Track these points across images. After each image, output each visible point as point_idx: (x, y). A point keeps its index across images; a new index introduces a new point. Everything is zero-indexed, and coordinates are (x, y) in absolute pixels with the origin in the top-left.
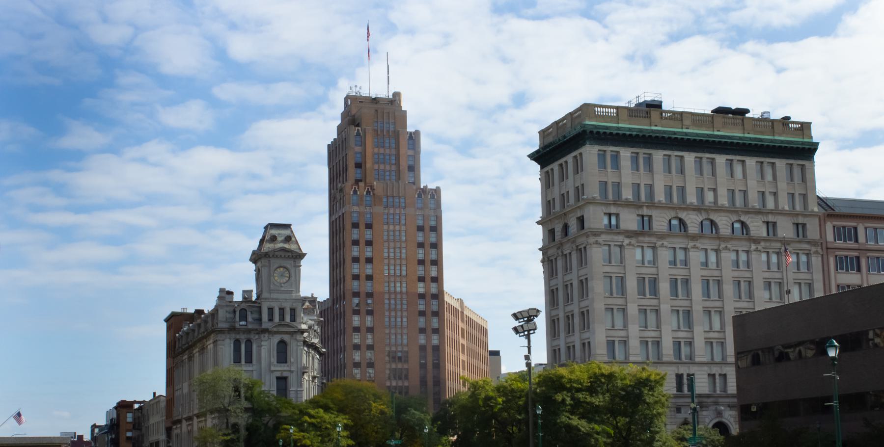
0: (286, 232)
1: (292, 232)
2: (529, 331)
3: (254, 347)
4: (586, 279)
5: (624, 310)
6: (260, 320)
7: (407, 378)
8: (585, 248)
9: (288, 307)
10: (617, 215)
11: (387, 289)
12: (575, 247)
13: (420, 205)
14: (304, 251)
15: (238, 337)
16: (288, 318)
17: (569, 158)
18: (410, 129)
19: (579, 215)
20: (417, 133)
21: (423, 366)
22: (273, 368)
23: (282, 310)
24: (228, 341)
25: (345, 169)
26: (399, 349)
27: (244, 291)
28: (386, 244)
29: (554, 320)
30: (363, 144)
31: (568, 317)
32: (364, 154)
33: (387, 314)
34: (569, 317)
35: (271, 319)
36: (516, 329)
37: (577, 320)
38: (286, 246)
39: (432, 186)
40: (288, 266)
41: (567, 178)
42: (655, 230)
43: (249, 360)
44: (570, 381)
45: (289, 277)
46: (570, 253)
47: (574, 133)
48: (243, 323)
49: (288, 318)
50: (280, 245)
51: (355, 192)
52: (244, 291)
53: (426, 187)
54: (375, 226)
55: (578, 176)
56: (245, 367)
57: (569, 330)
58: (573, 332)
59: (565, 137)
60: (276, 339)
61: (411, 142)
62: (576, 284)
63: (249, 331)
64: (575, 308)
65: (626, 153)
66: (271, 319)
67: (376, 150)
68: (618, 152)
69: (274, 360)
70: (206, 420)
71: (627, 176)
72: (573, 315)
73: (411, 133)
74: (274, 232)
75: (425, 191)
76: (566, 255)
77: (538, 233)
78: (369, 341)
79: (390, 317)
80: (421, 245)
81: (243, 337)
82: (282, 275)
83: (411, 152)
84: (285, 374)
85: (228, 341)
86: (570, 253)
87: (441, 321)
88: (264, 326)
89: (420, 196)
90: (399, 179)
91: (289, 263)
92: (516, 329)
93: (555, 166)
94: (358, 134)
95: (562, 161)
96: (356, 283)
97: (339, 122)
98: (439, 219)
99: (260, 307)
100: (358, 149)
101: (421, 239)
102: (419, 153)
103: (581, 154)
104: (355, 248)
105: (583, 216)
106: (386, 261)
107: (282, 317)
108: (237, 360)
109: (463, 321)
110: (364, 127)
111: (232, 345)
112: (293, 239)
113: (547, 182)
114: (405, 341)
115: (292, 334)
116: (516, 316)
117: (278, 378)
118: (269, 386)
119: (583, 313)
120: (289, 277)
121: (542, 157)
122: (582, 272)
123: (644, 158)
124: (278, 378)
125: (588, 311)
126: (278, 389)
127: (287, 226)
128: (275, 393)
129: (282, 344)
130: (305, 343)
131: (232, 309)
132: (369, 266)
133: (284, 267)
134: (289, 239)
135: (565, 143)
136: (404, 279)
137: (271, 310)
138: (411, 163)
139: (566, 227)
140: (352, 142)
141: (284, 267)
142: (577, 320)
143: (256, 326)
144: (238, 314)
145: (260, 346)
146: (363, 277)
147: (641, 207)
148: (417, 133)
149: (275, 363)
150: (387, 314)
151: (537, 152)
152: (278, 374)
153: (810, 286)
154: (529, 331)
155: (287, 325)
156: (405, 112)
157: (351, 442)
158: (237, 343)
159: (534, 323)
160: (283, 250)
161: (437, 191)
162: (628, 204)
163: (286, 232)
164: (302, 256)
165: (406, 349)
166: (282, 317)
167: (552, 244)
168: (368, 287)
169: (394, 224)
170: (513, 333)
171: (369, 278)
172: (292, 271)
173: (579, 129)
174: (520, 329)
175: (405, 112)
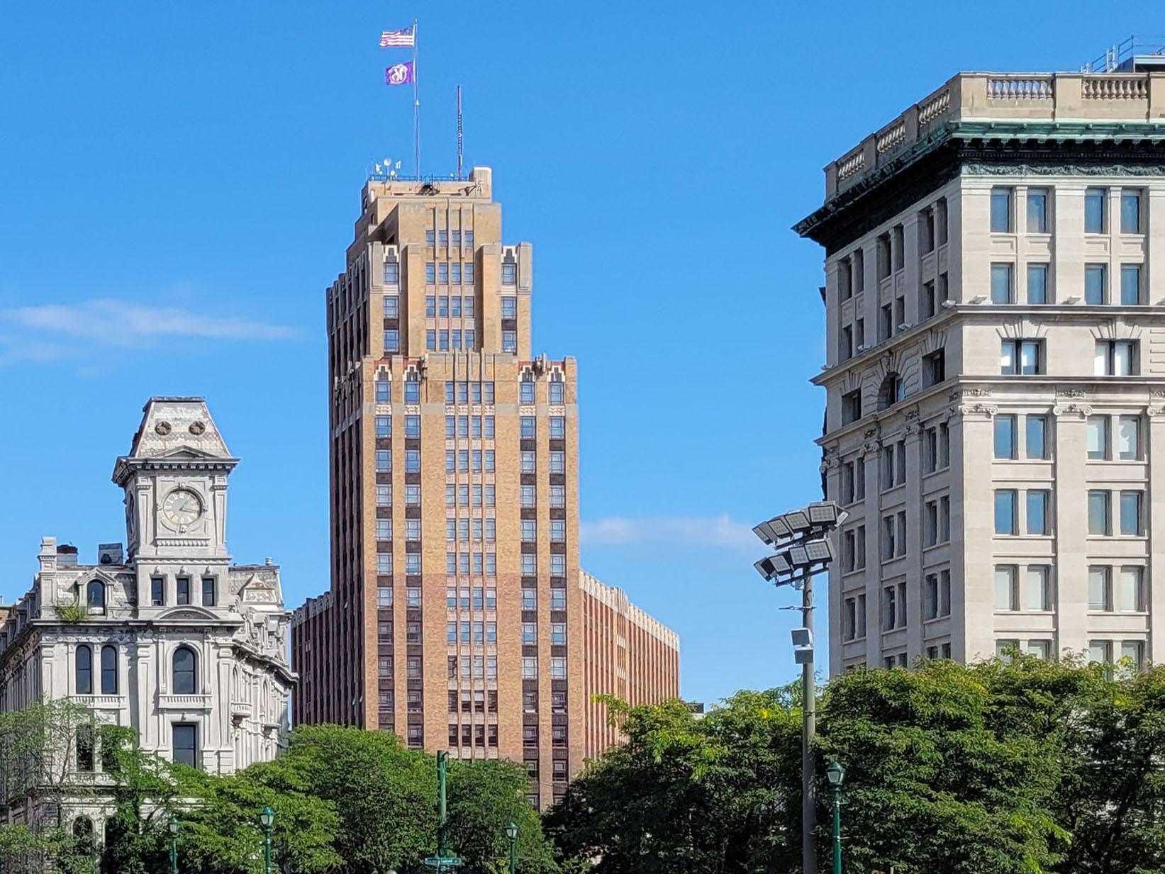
2: (806, 567)
3: (123, 660)
4: (946, 499)
5: (1049, 573)
7: (494, 741)
8: (944, 426)
9: (196, 573)
10: (1039, 344)
12: (915, 427)
15: (83, 639)
16: (197, 599)
17: (909, 218)
19: (931, 348)
21: (531, 723)
22: (162, 704)
23: (184, 582)
25: (364, 334)
26: (479, 686)
27: (101, 547)
29: (850, 602)
31: (889, 591)
34: (893, 594)
36: (767, 566)
37: (915, 595)
38: (193, 444)
40: (198, 487)
41: (901, 265)
42: (1143, 374)
43: (111, 686)
44: (935, 697)
45: (201, 511)
46: (901, 444)
47: (927, 148)
48: (99, 610)
49: (197, 599)
51: (383, 375)
52: (101, 547)
54: (425, 444)
55: (928, 257)
56: (100, 701)
57: (893, 618)
58: (904, 622)
59: (899, 164)
60: (169, 646)
62: (914, 512)
63: (108, 628)
64: (911, 570)
65: (1070, 190)
67: (431, 291)
68: (1049, 190)
69: (167, 686)
70: (25, 812)
71: (1075, 247)
72: (903, 586)
76: (889, 450)
77: (817, 405)
81: (97, 640)
84: (190, 717)
86: (901, 444)
88: (143, 616)
90: (482, 345)
92: (767, 566)
93: (868, 243)
94: (390, 261)
95: (888, 226)
99: (135, 577)
103: (942, 202)
105: (942, 352)
109: (621, 630)
110: (403, 241)
111: (73, 657)
113: (848, 281)
115: (201, 631)
116: (766, 532)
117: (175, 725)
118: (157, 739)
119: (931, 580)
120: (201, 511)
121: (832, 227)
122: (933, 484)
123: (1123, 197)
124: (175, 725)
125: (946, 573)
126: (176, 748)
128: (169, 757)
129: (184, 652)
130: (239, 652)
133: (188, 491)
135: (899, 180)
137: (159, 582)
139: (891, 386)
140: (378, 275)
141: (188, 491)
142: (915, 595)
143: (126, 616)
144: (83, 591)
145: (134, 660)
147: (1109, 320)
149: (170, 693)
151: (819, 214)
152: (177, 717)
154: (806, 567)
155: (196, 614)
157: (337, 860)
158: (84, 651)
160: (189, 453)
162: (1070, 316)
165: (492, 686)
167: (853, 426)
170: (758, 575)
173: (939, 138)
174: (780, 564)
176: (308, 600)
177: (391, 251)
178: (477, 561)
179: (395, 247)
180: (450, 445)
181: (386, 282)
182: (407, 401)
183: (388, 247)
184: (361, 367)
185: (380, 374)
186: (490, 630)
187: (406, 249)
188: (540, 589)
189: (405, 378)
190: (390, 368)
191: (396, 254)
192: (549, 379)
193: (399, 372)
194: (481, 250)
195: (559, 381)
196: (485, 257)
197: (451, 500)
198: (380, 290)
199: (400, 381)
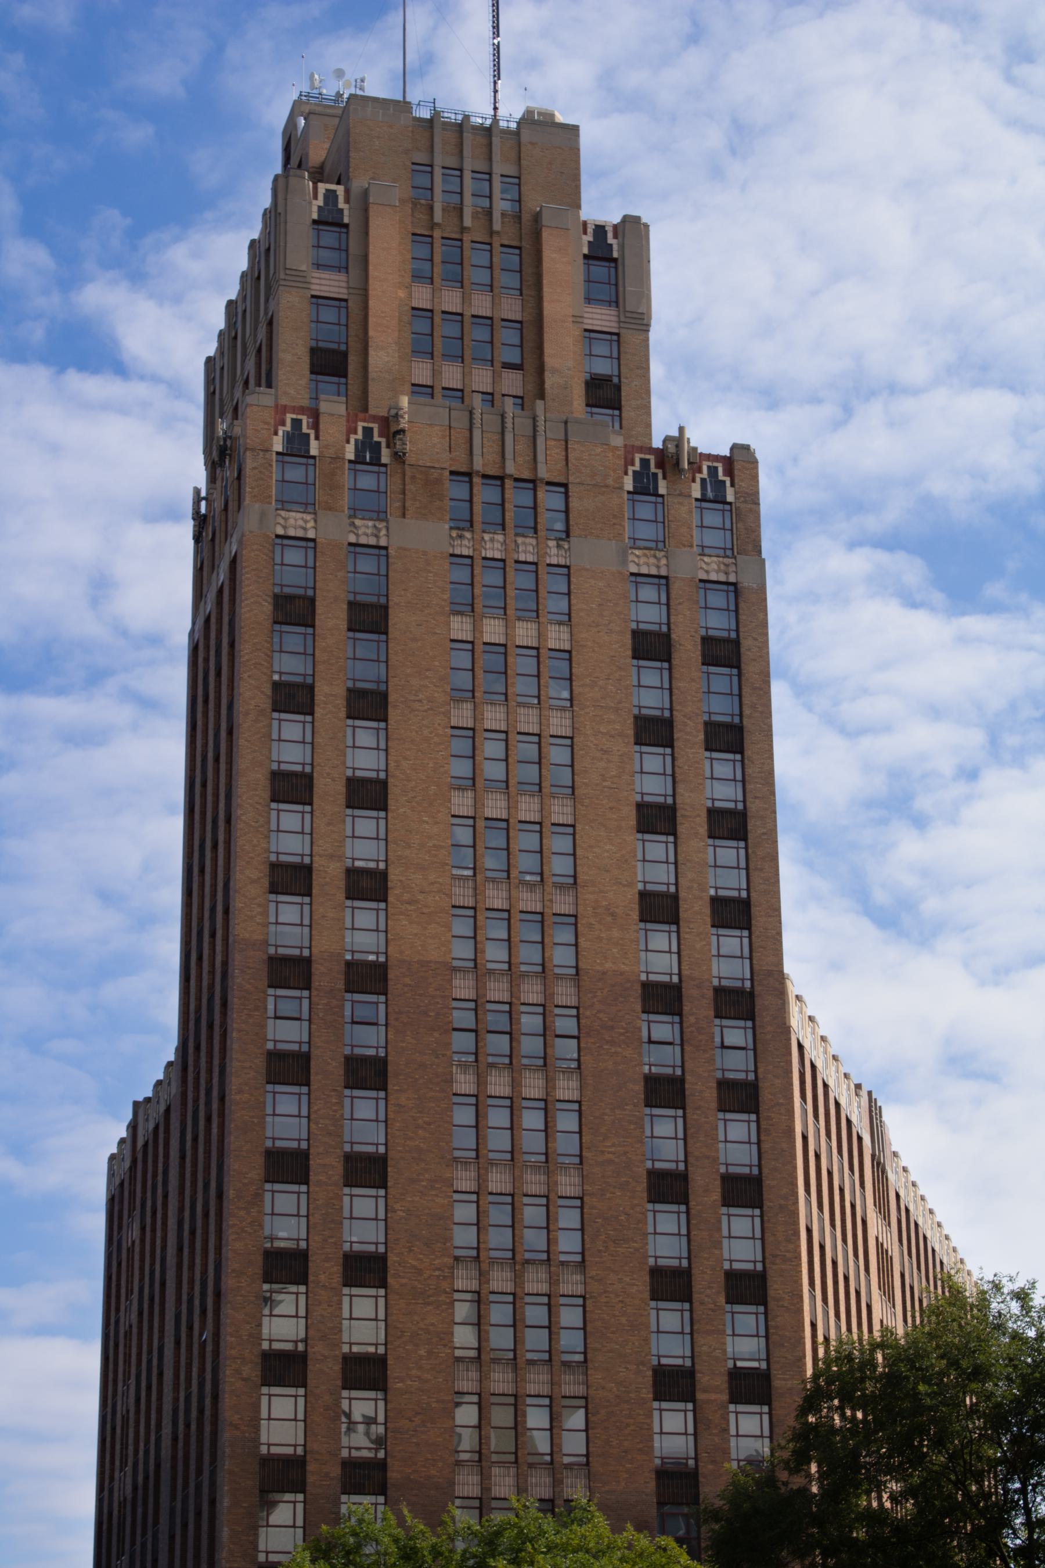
11: (463, 951)
13: (646, 531)
18: (599, 207)
20: (633, 229)
28: (464, 1280)
30: (355, 262)
32: (354, 309)
33: (465, 1083)
39: (710, 435)
53: (678, 441)
54: (398, 619)
61: (600, 270)
67: (422, 296)
73: (600, 230)
75: (672, 459)
78: (363, 1234)
79: (479, 1102)
80: (665, 1091)
83: (601, 318)
87: (762, 866)
89: (645, 487)
96: (289, 910)
97: (233, 293)
98: (744, 597)
100: (330, 284)
101: (669, 1153)
102: (641, 322)
104: (285, 1199)
106: (464, 1280)
110: (359, 183)
114: (568, 1244)
132: (366, 823)
136: (570, 1385)
138: (603, 367)
146: (329, 788)
150: (465, 1083)
161: (739, 462)
168: (362, 932)
169: (512, 1062)
171: (368, 885)
176: (136, 1105)
177: (331, 196)
178: (531, 841)
179: (340, 190)
180: (460, 627)
181: (318, 266)
182: (354, 512)
183: (322, 187)
184: (244, 429)
185: (289, 438)
186: (558, 755)
187: (366, 193)
188: (690, 1020)
189: (350, 453)
190: (316, 426)
191: (341, 204)
192: (697, 493)
193: (336, 438)
194: (537, 218)
195: (720, 500)
196: (545, 234)
197: (462, 768)
198: (301, 279)
199: (339, 458)
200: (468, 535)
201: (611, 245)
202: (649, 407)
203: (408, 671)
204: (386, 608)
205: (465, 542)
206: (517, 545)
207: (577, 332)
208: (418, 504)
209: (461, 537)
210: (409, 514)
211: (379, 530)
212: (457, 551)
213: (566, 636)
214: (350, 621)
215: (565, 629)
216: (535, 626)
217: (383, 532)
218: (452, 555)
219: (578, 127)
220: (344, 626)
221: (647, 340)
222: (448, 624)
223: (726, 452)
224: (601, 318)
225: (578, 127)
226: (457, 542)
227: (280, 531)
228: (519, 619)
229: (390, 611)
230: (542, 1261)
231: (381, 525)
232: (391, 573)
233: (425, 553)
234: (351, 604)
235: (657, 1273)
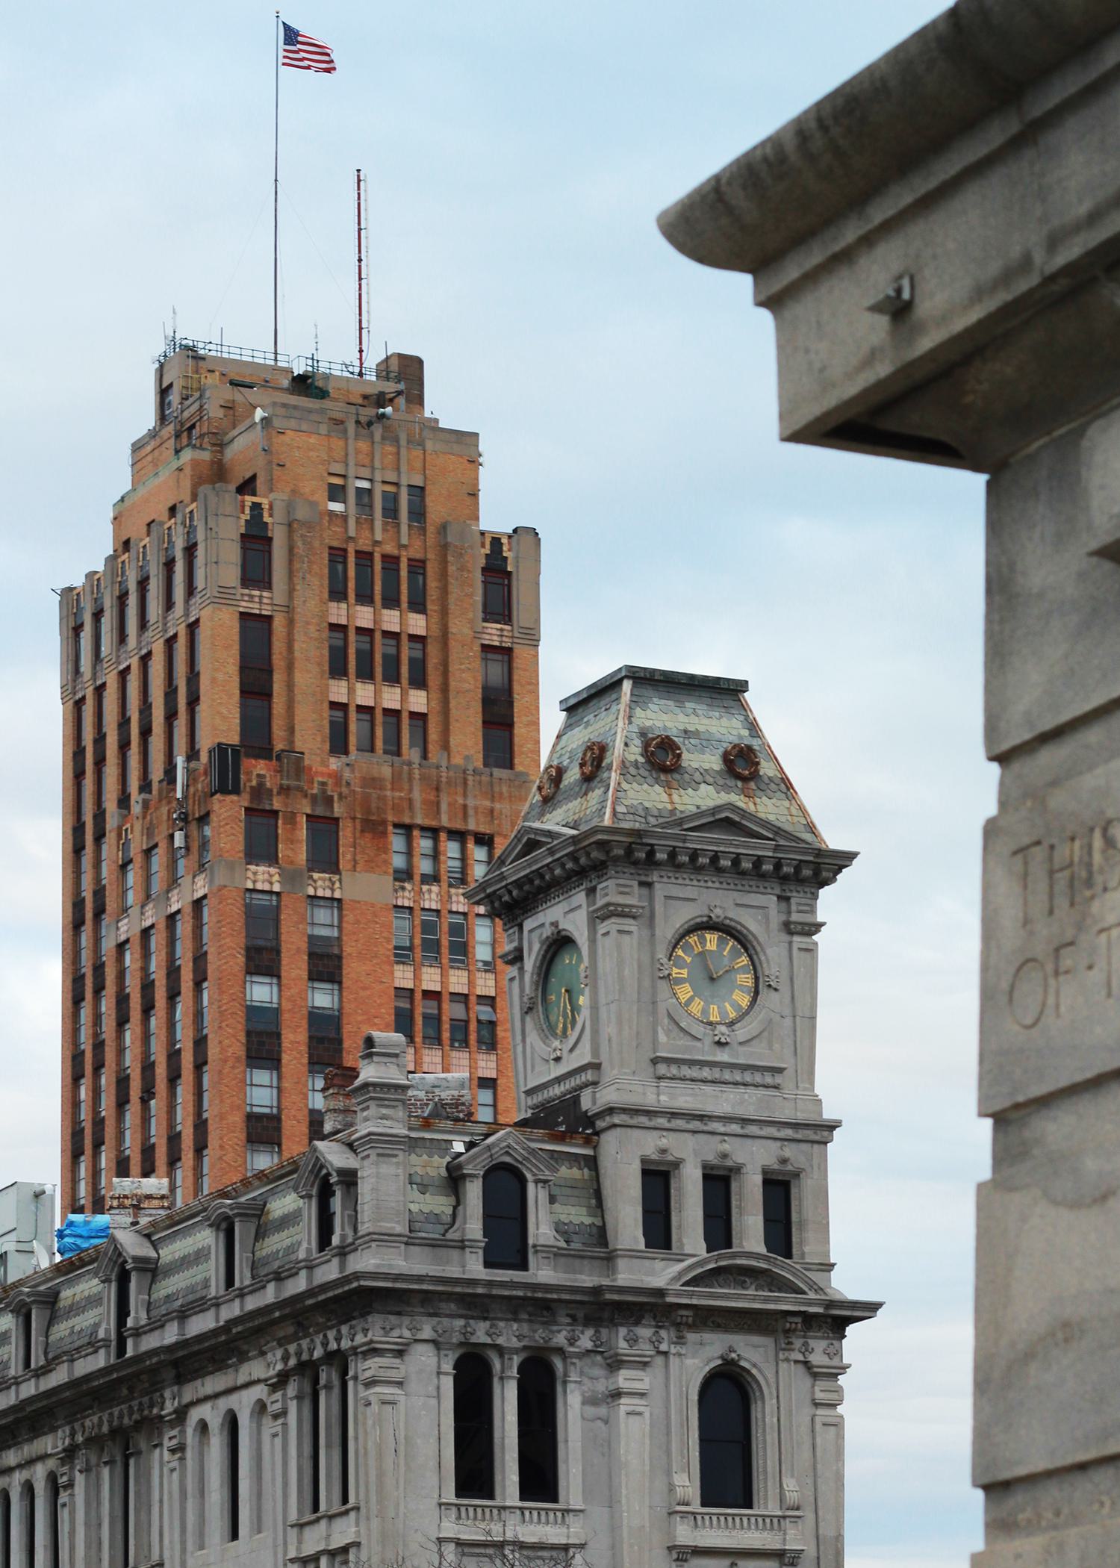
0: (725, 728)
1: (753, 727)
6: (598, 1241)
14: (834, 840)
15: (481, 1333)
18: (496, 515)
23: (719, 1183)
24: (423, 1357)
35: (659, 1231)
40: (750, 922)
50: (705, 797)
60: (696, 1359)
63: (540, 1306)
66: (659, 1231)
69: (688, 1484)
73: (496, 542)
74: (664, 717)
82: (712, 978)
83: (493, 633)
85: (423, 1357)
91: (757, 911)
107: (719, 1227)
108: (474, 1477)
111: (448, 1384)
112: (766, 769)
127: (727, 692)
131: (438, 1166)
134: (744, 763)
137: (658, 1179)
148: (526, 536)
153: (681, 1368)
156: (465, 443)
159: (839, 1390)
163: (725, 728)
164: (823, 866)
166: (719, 1227)
172: (774, 952)
175: (465, 443)
200: (408, 886)
201: (506, 558)
202: (538, 724)
203: (360, 1018)
204: (339, 958)
205: (407, 894)
206: (450, 897)
207: (477, 648)
208: (366, 858)
209: (403, 888)
210: (359, 868)
211: (333, 883)
212: (400, 903)
213: (492, 983)
214: (310, 972)
215: (491, 976)
216: (466, 974)
217: (337, 885)
218: (396, 906)
219: (477, 435)
220: (305, 975)
221: (536, 656)
222: (392, 973)
223: (989, 1122)
224: (493, 633)
225: (477, 435)
226: (400, 893)
227: (250, 886)
228: (452, 967)
229: (344, 961)
230: (254, 1215)
231: (336, 878)
232: (345, 925)
233: (373, 905)
234: (311, 955)
235: (252, 1118)
